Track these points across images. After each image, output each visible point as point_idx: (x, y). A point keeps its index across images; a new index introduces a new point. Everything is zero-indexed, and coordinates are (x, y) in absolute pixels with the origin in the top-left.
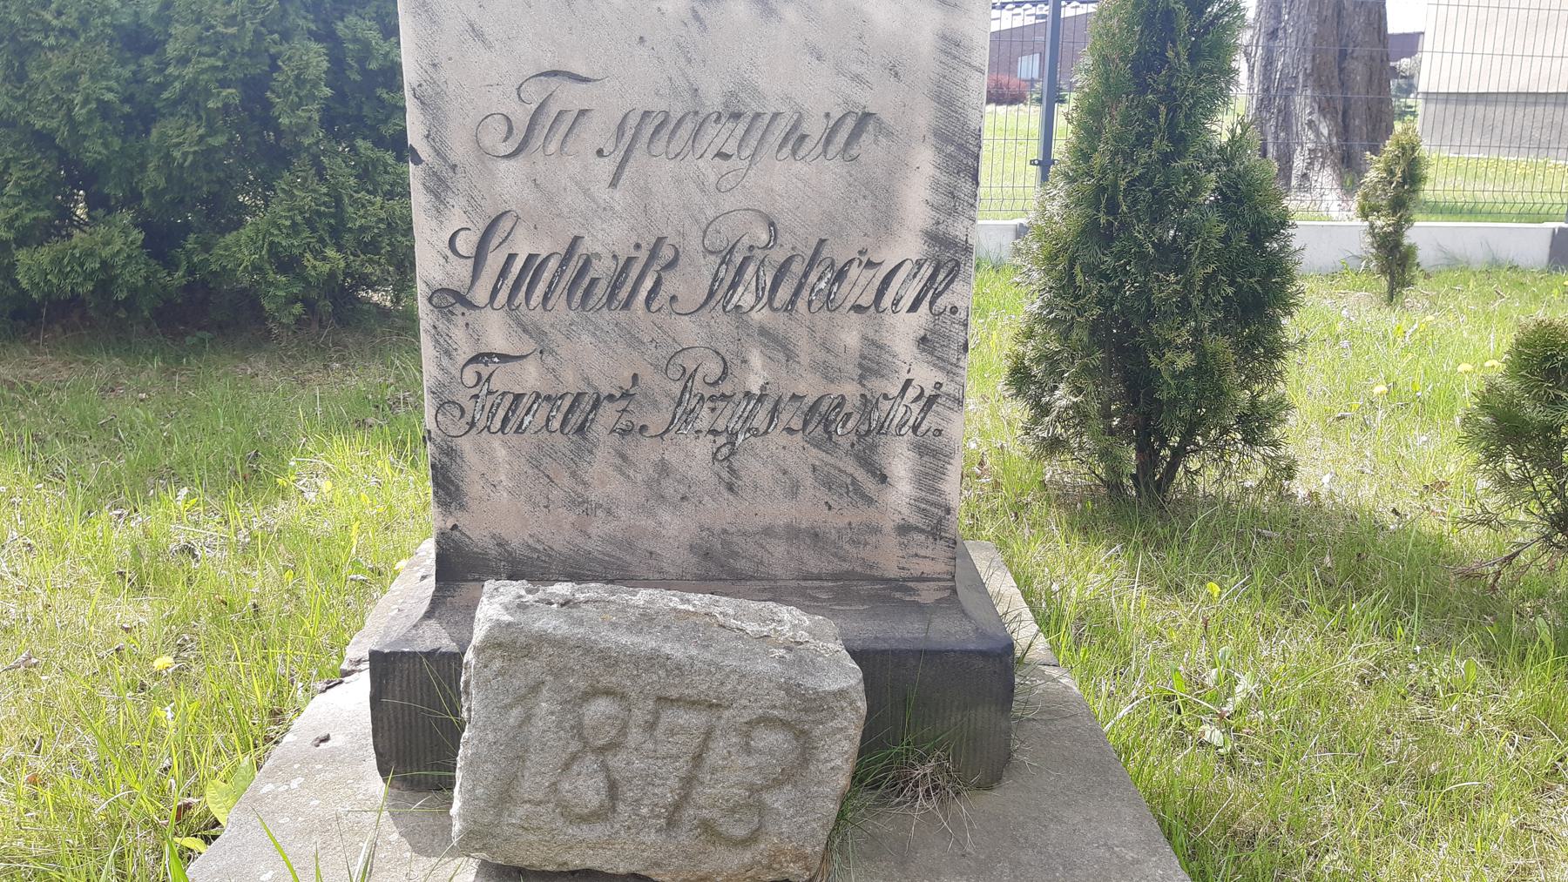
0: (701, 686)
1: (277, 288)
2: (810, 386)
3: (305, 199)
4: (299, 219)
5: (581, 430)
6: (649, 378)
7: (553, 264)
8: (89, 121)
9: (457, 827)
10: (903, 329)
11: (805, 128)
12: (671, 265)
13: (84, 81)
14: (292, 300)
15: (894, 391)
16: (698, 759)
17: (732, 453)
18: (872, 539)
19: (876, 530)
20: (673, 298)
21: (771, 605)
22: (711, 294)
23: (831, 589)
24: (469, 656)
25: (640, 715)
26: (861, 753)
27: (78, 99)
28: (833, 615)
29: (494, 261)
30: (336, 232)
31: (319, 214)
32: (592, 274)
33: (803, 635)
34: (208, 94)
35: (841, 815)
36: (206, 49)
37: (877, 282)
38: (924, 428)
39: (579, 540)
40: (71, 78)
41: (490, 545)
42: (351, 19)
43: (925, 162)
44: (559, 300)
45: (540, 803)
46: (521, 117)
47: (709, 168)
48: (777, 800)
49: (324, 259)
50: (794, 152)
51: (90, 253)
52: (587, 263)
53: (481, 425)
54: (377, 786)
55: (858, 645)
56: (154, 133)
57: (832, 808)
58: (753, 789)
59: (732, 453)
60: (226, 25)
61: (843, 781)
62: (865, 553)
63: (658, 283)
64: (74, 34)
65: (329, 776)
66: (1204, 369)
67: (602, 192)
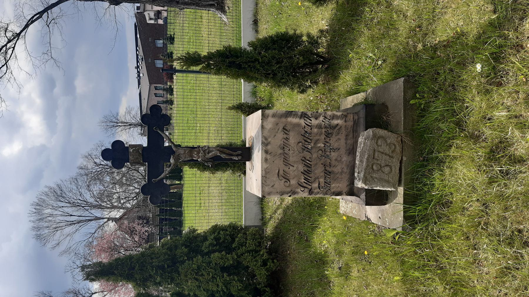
0: (372, 152)
1: (271, 265)
2: (323, 137)
4: (254, 260)
5: (330, 173)
6: (322, 162)
7: (305, 176)
9: (393, 189)
10: (314, 122)
11: (285, 137)
12: (305, 158)
14: (273, 262)
15: (324, 123)
16: (382, 153)
17: (333, 149)
18: (347, 126)
19: (346, 126)
20: (310, 158)
21: (358, 143)
22: (309, 152)
23: (355, 133)
24: (366, 188)
26: (382, 128)
28: (359, 133)
29: (305, 185)
30: (256, 252)
31: (252, 256)
32: (306, 170)
33: (363, 138)
35: (391, 132)
36: (215, 281)
37: (307, 126)
38: (329, 118)
39: (347, 173)
41: (348, 187)
42: (203, 248)
43: (290, 119)
44: (310, 175)
45: (389, 177)
46: (284, 180)
47: (291, 152)
48: (389, 141)
49: (263, 254)
50: (289, 139)
52: (305, 171)
53: (329, 188)
54: (387, 206)
55: (365, 129)
56: (234, 293)
57: (390, 133)
58: (387, 145)
59: (333, 149)
61: (386, 131)
62: (349, 127)
63: (308, 160)
65: (386, 214)
66: (301, 53)
67: (295, 168)
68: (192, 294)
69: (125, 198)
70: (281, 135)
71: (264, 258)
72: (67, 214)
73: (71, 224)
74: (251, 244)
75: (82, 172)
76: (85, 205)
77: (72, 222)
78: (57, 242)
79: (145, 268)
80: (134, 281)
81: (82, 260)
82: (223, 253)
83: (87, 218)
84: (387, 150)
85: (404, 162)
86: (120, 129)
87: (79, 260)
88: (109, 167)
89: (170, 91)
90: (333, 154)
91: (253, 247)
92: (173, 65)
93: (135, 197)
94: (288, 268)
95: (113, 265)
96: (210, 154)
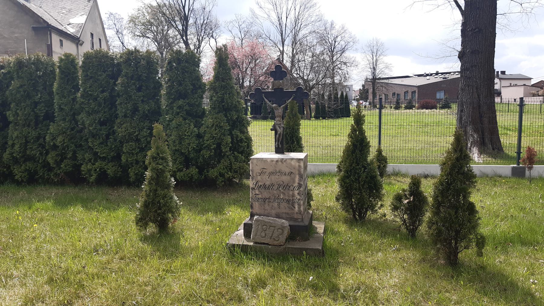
2: (287, 198)
3: (226, 164)
6: (271, 197)
8: (191, 151)
13: (191, 144)
14: (222, 182)
19: (294, 213)
25: (268, 227)
27: (190, 147)
29: (257, 185)
30: (230, 169)
34: (211, 146)
36: (211, 138)
40: (189, 144)
42: (235, 130)
43: (297, 176)
46: (260, 172)
47: (277, 177)
48: (280, 236)
51: (189, 173)
54: (244, 238)
58: (278, 235)
60: (215, 135)
64: (190, 136)
67: (267, 179)
68: (203, 122)
69: (299, 67)
70: (287, 170)
71: (226, 174)
72: (288, 14)
73: (279, 17)
74: (236, 165)
75: (328, 25)
76: (296, 29)
77: (280, 18)
78: (263, 6)
79: (222, 89)
80: (214, 81)
81: (246, 29)
82: (231, 145)
83: (284, 32)
84: (275, 235)
85: (268, 246)
86: (369, 58)
87: (245, 26)
88: (332, 49)
89: (410, 106)
90: (276, 204)
91: (234, 167)
92: (436, 109)
93: (300, 76)
94: (217, 193)
95: (226, 66)
96: (278, 128)
